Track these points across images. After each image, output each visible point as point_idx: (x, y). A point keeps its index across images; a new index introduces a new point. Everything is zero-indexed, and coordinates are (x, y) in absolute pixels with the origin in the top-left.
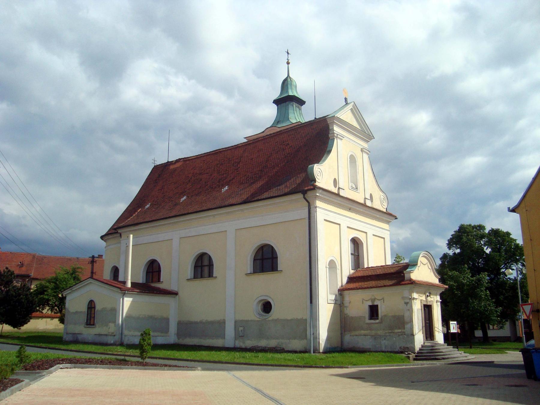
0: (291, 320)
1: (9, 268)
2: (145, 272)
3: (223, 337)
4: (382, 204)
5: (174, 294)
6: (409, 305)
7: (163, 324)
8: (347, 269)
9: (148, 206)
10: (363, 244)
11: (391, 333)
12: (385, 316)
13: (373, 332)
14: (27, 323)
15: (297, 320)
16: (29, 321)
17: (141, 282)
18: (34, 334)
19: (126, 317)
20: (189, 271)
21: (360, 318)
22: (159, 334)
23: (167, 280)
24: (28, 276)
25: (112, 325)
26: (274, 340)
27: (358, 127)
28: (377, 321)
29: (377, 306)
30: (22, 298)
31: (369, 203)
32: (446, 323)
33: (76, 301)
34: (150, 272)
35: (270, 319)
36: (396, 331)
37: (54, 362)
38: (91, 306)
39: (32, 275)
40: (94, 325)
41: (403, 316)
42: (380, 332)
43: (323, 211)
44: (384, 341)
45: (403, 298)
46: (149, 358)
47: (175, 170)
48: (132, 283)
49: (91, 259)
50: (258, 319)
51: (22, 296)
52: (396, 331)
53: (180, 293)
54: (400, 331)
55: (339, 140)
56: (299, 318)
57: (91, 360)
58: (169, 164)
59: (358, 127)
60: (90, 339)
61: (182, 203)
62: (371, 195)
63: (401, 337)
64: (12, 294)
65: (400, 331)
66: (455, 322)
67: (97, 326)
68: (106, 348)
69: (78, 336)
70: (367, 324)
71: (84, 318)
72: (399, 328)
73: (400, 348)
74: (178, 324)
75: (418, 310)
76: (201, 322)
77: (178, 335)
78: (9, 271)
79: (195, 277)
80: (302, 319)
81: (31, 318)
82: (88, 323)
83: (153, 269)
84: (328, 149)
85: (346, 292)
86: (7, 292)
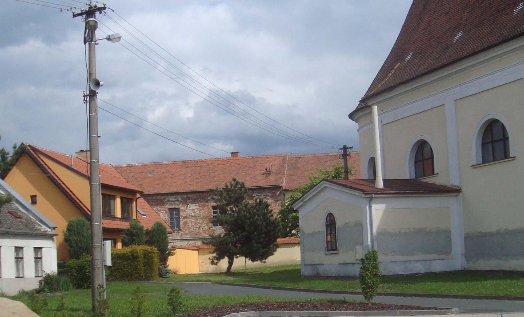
1: (237, 179)
2: (413, 161)
5: (455, 191)
7: (441, 241)
9: (409, 57)
14: (272, 254)
16: (276, 251)
17: (408, 177)
18: (290, 268)
19: (378, 234)
20: (473, 150)
23: (445, 172)
24: (279, 188)
25: (358, 248)
30: (257, 220)
33: (311, 218)
34: (419, 161)
37: (231, 308)
38: (331, 222)
39: (284, 185)
40: (336, 250)
46: (379, 294)
48: (385, 181)
49: (342, 152)
51: (257, 217)
53: (464, 189)
57: (287, 304)
60: (333, 271)
61: (455, 43)
64: (245, 216)
67: (341, 251)
68: (347, 283)
69: (318, 267)
71: (323, 240)
74: (465, 238)
76: (498, 233)
77: (467, 256)
78: (237, 183)
79: (485, 160)
81: (277, 246)
82: (330, 248)
83: (423, 155)
86: (239, 212)
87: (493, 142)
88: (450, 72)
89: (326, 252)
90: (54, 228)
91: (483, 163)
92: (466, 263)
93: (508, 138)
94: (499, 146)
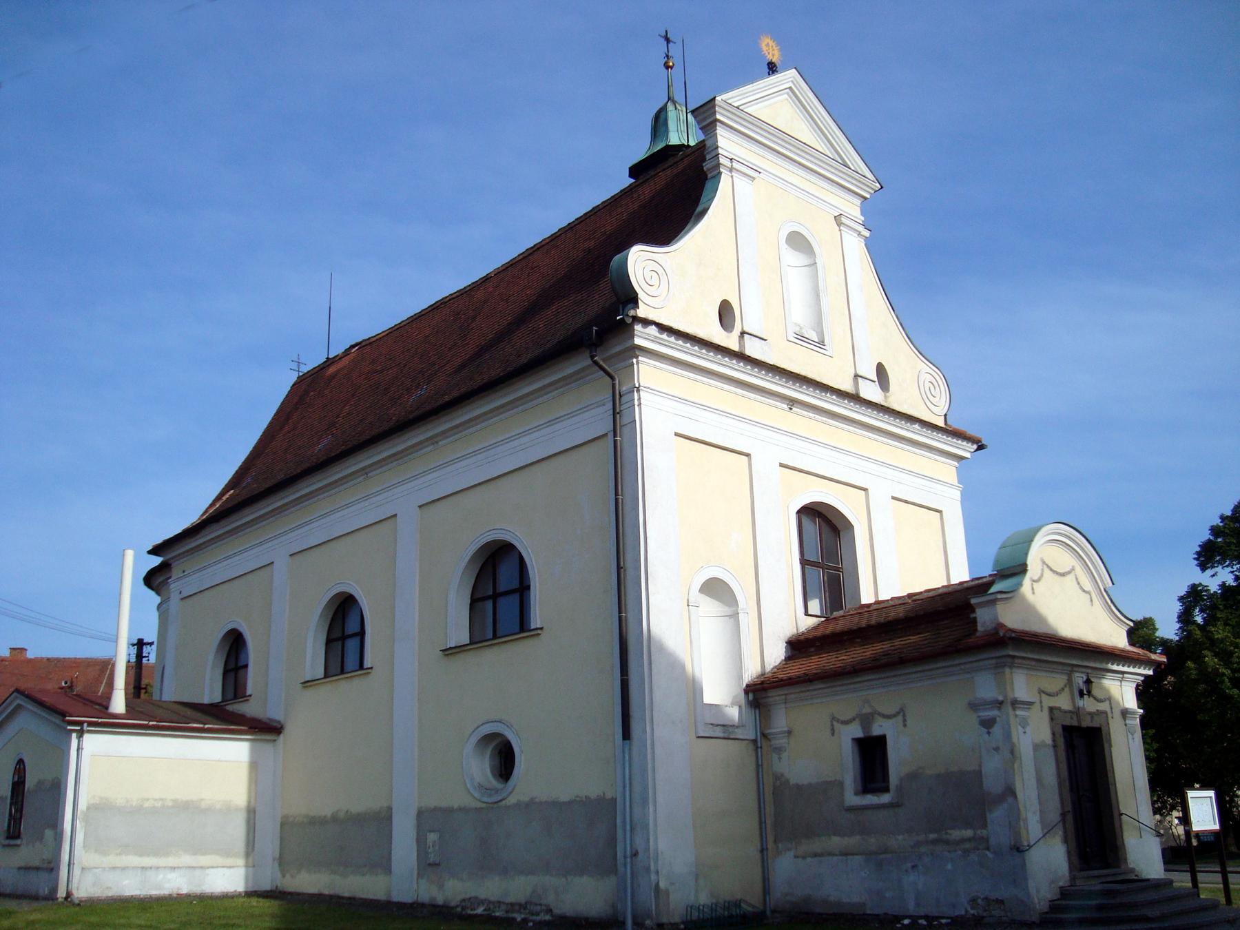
0: (570, 803)
3: (385, 865)
4: (927, 399)
6: (996, 729)
8: (783, 610)
10: (849, 526)
11: (934, 842)
12: (913, 776)
13: (873, 842)
15: (586, 802)
21: (831, 787)
22: (217, 860)
26: (523, 878)
27: (821, 146)
28: (885, 798)
29: (882, 740)
31: (871, 392)
32: (1168, 789)
35: (512, 800)
36: (956, 834)
41: (979, 774)
42: (899, 841)
43: (665, 400)
44: (912, 877)
45: (974, 706)
47: (333, 376)
50: (479, 805)
52: (956, 834)
54: (969, 833)
55: (740, 181)
56: (593, 796)
58: (330, 362)
59: (821, 146)
62: (881, 370)
63: (974, 857)
65: (969, 833)
66: (1211, 793)
70: (851, 809)
72: (967, 825)
73: (973, 901)
74: (282, 825)
75: (1036, 747)
77: (428, 865)
79: (477, 640)
80: (601, 800)
84: (699, 209)
85: (775, 696)
87: (495, 597)
88: (286, 501)
89: (7, 842)
90: (798, 241)
91: (326, 677)
92: (279, 875)
93: (529, 587)
94: (508, 606)
